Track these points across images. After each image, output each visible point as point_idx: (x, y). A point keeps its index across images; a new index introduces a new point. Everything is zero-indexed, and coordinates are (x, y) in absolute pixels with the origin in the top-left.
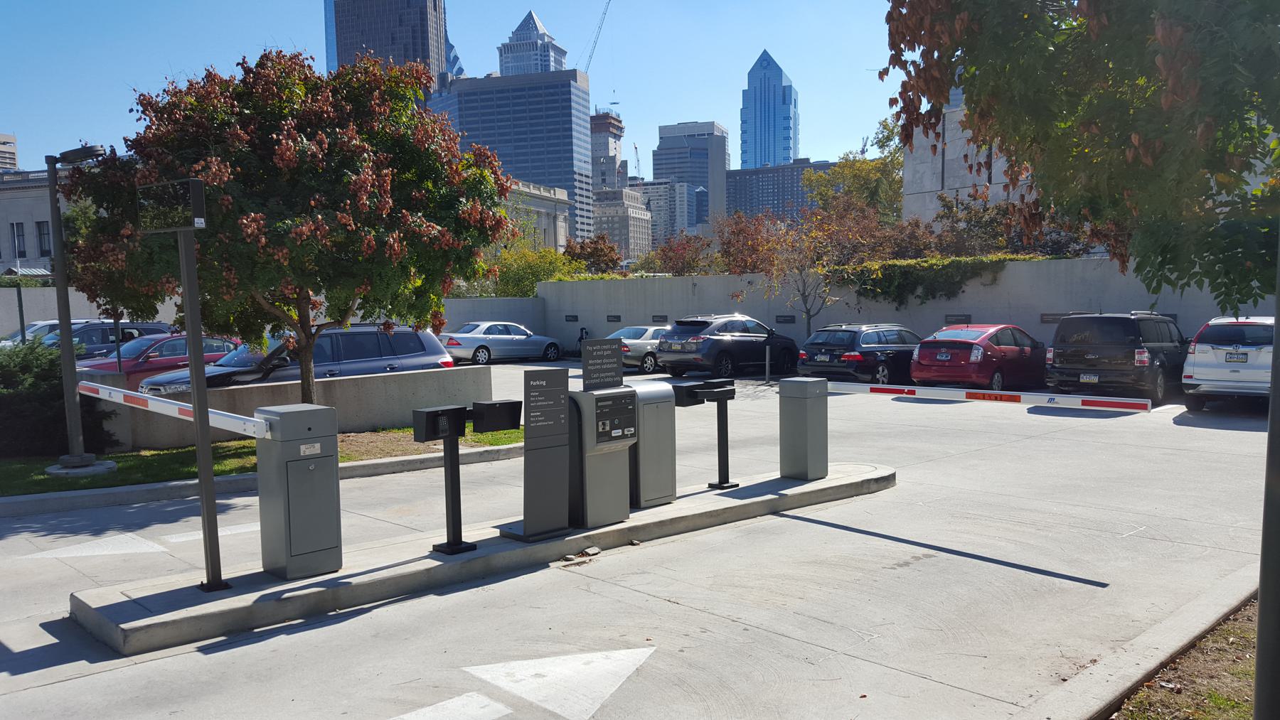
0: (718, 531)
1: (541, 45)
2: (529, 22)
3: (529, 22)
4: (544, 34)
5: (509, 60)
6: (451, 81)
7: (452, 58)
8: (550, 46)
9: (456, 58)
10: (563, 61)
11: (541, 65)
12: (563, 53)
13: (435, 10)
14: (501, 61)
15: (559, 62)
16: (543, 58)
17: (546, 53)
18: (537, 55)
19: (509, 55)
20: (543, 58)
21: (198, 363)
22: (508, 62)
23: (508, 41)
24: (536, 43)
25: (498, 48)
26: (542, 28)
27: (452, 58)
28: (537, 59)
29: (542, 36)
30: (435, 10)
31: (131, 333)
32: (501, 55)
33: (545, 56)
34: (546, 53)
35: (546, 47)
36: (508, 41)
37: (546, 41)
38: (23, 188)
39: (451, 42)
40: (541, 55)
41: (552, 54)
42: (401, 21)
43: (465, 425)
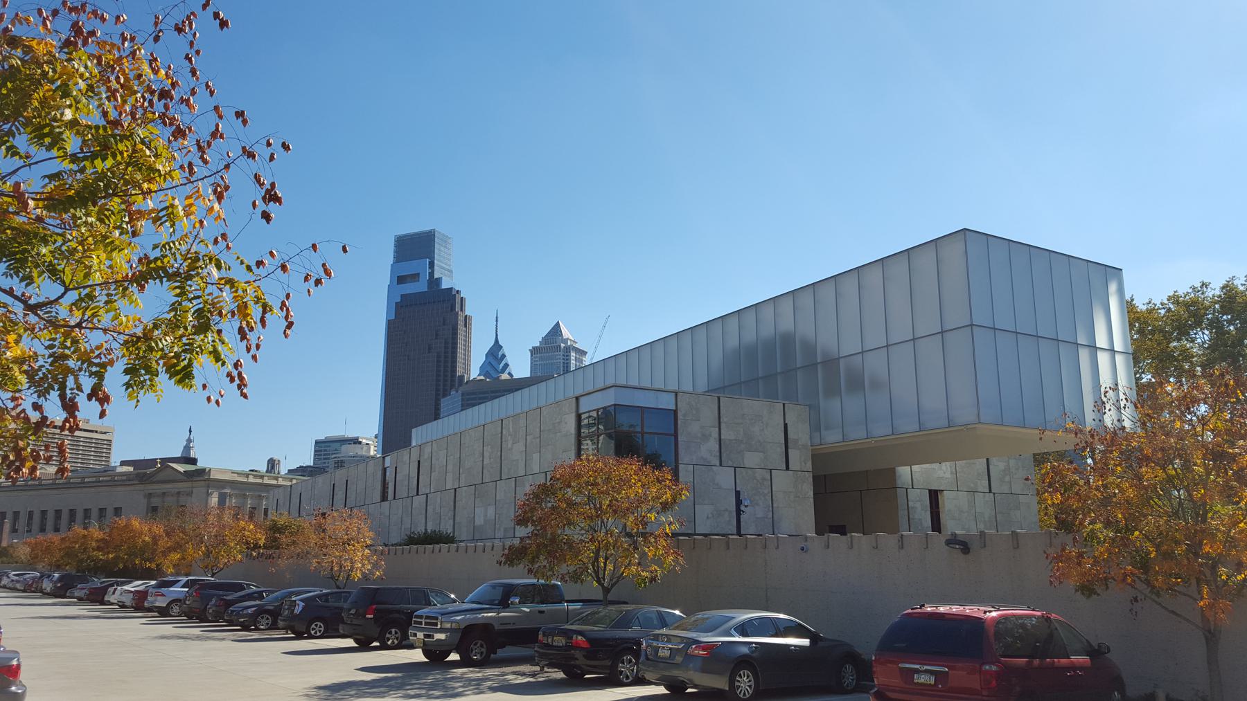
0: (569, 697)
1: (564, 347)
2: (556, 330)
3: (556, 330)
4: (568, 339)
5: (538, 359)
6: (467, 382)
7: (500, 356)
8: (571, 348)
9: (503, 356)
10: (584, 359)
11: (564, 363)
12: (584, 353)
13: (465, 326)
14: (531, 359)
15: (578, 360)
16: (565, 358)
17: (568, 354)
18: (560, 355)
19: (538, 355)
20: (565, 358)
21: (130, 356)
22: (537, 361)
23: (538, 345)
24: (560, 346)
25: (530, 350)
26: (566, 333)
27: (500, 356)
28: (560, 359)
29: (566, 341)
30: (465, 326)
31: (116, 154)
32: (532, 355)
33: (567, 356)
34: (568, 354)
35: (568, 350)
36: (538, 345)
37: (569, 344)
38: (21, 490)
39: (500, 343)
40: (563, 355)
41: (572, 354)
42: (437, 335)
43: (192, 458)
